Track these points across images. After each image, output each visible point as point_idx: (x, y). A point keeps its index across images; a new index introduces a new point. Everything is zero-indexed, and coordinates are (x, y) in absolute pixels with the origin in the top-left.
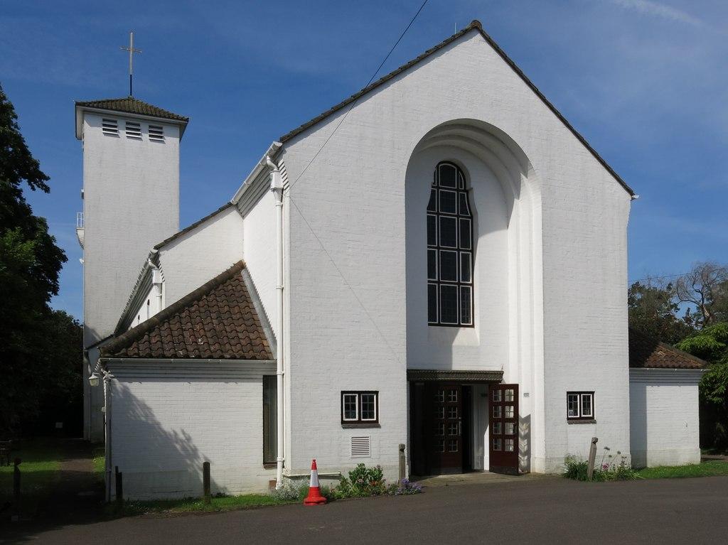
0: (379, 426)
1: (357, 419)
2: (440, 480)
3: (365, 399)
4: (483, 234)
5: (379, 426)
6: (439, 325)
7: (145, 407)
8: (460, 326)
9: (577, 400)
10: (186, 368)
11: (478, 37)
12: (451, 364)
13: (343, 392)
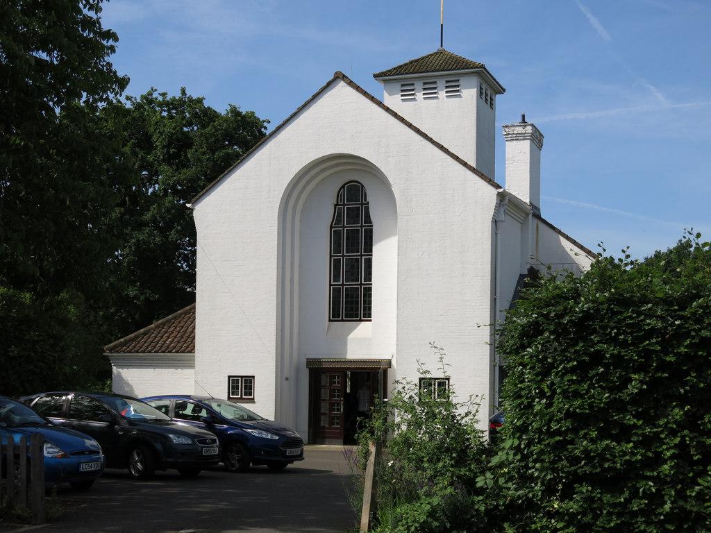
0: (254, 402)
1: (239, 396)
2: (322, 448)
3: (246, 382)
4: (380, 240)
5: (254, 402)
6: (342, 320)
7: (128, 384)
8: (361, 321)
9: (232, 386)
10: (152, 360)
11: (342, 84)
12: (346, 353)
13: (229, 377)
